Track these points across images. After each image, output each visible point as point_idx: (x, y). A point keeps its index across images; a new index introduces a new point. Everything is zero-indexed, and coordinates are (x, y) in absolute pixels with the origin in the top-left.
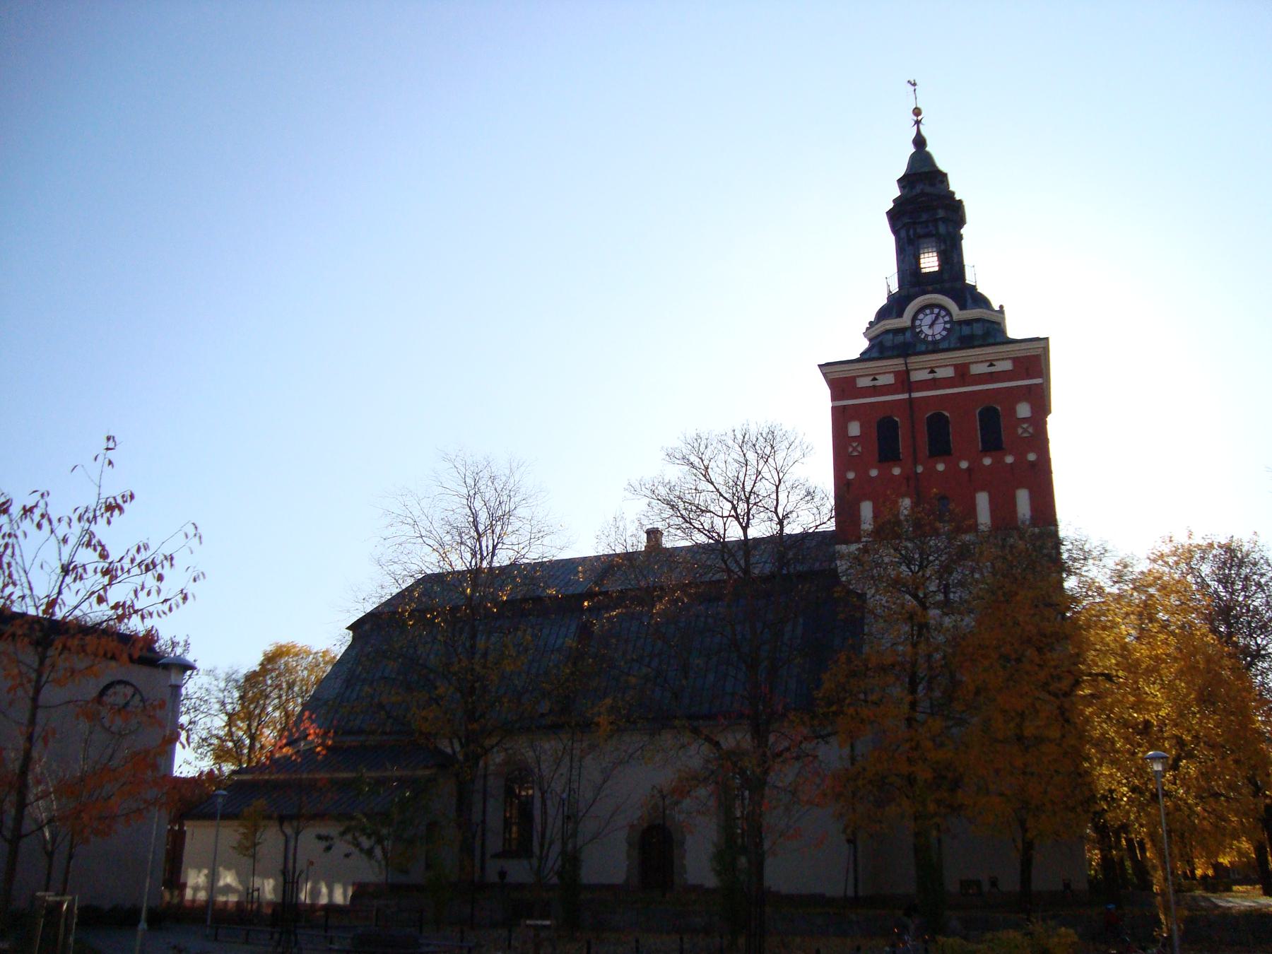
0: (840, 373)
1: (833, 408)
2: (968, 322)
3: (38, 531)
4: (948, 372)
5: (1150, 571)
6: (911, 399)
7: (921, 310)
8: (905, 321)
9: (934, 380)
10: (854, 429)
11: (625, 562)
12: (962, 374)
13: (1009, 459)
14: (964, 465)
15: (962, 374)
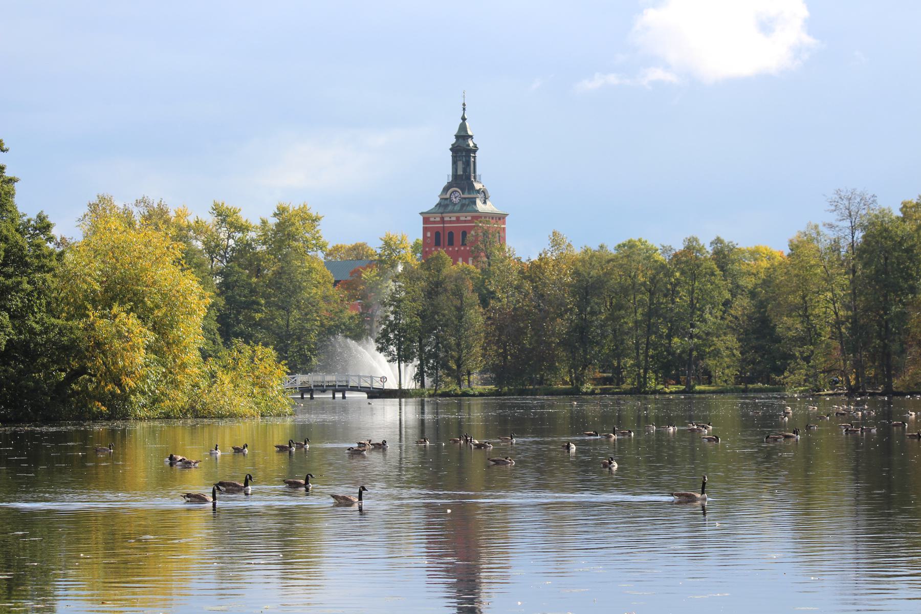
0: (504, 218)
1: (423, 227)
2: (465, 198)
3: (719, 236)
4: (454, 219)
5: (177, 342)
6: (444, 227)
7: (453, 192)
8: (448, 196)
9: (450, 221)
10: (429, 234)
11: (414, 319)
12: (458, 220)
13: (468, 248)
14: (456, 249)
15: (458, 220)
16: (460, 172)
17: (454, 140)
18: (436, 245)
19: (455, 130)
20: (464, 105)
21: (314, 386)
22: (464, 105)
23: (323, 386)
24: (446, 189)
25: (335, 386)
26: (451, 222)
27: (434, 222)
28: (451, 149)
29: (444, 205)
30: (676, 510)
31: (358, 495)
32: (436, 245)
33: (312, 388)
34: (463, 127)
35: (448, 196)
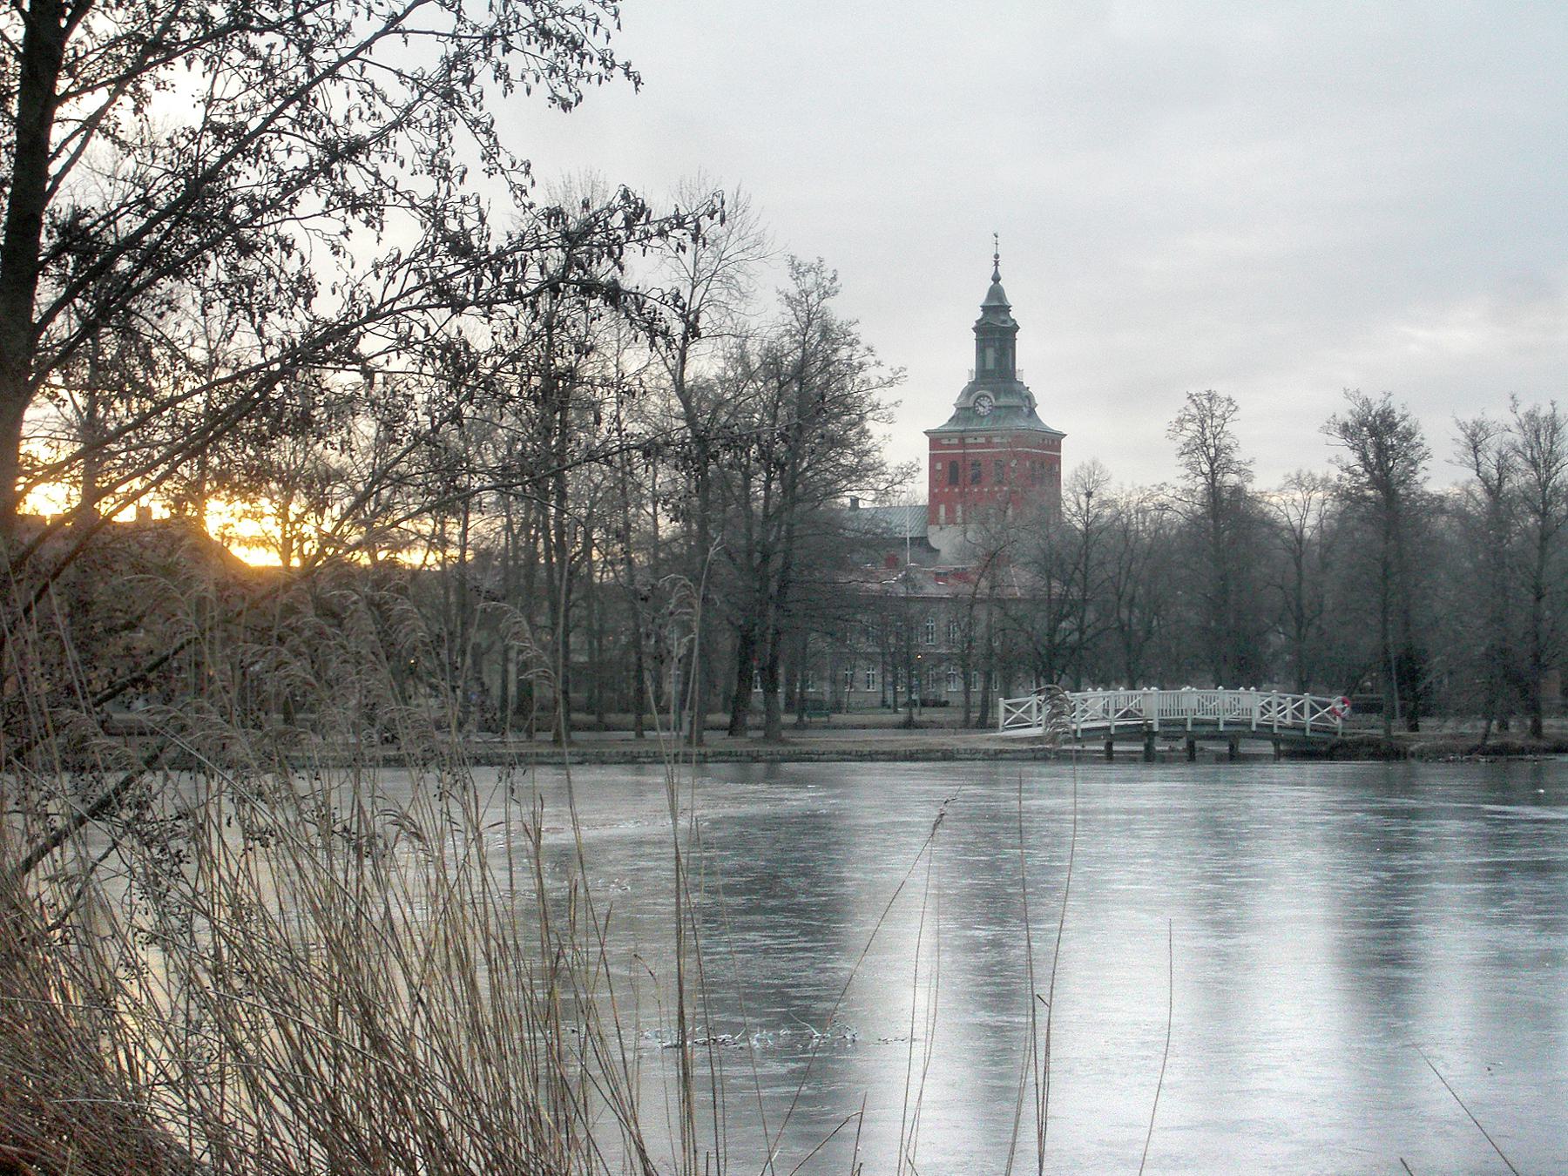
8: (971, 404)
10: (939, 466)
16: (990, 365)
17: (980, 314)
18: (950, 484)
19: (981, 297)
20: (997, 256)
21: (1163, 724)
22: (997, 256)
23: (1216, 724)
24: (968, 392)
25: (1216, 724)
26: (976, 446)
27: (949, 447)
28: (975, 329)
29: (965, 412)
30: (1468, 923)
31: (674, 933)
32: (950, 484)
33: (1156, 729)
34: (996, 293)
35: (971, 404)
